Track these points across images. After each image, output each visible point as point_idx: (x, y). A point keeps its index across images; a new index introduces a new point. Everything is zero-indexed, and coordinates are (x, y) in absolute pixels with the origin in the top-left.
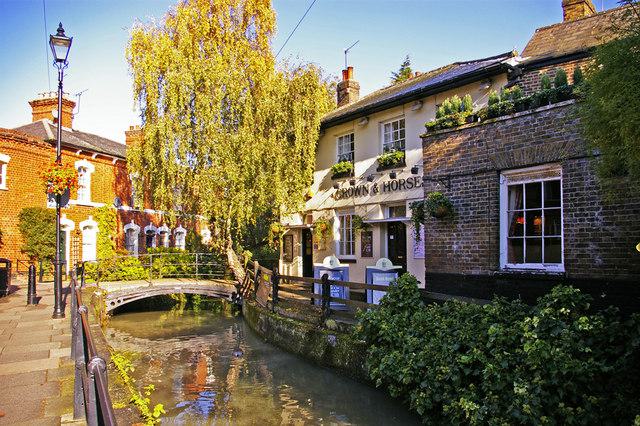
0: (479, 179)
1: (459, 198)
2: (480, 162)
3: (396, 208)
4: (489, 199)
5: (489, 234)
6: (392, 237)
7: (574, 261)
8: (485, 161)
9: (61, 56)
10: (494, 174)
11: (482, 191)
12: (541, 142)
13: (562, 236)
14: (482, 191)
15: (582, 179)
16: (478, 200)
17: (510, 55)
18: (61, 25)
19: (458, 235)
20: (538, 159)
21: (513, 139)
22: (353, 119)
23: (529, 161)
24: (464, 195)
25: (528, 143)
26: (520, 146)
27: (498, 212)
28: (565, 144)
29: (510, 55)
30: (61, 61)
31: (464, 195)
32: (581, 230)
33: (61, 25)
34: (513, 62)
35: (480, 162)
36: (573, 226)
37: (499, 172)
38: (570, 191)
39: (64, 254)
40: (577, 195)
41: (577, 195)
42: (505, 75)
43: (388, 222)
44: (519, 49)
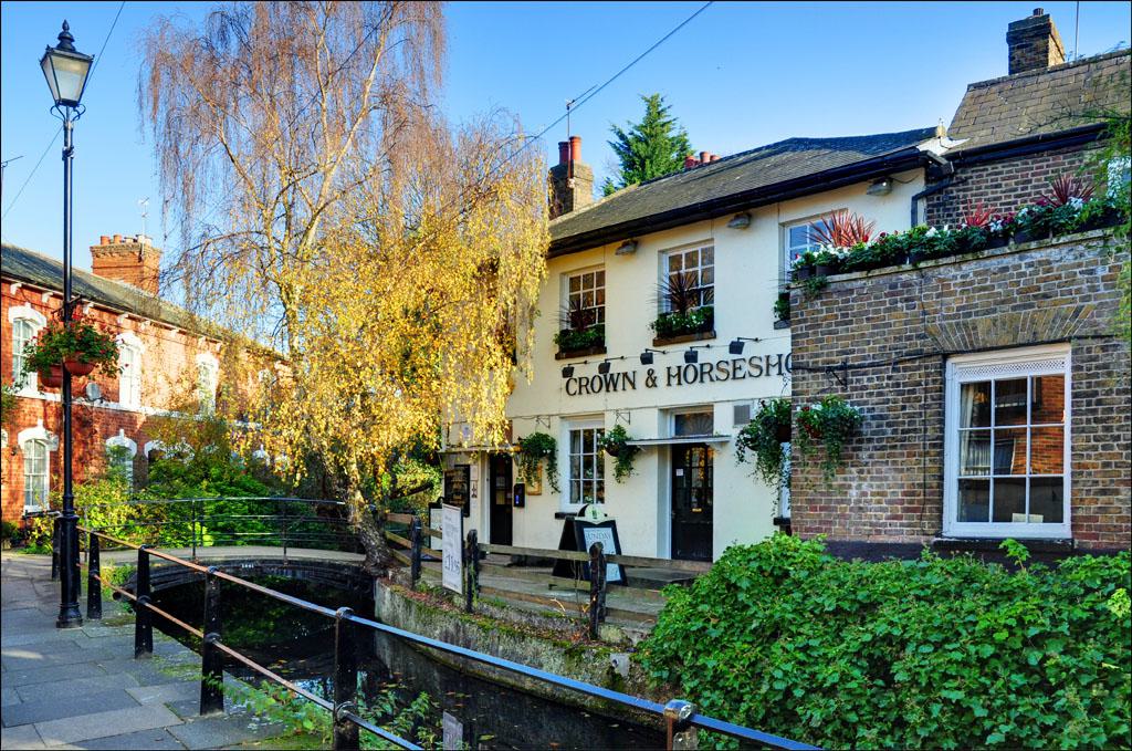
0: (905, 369)
1: (866, 403)
2: (909, 338)
3: (694, 419)
4: (925, 407)
5: (925, 470)
6: (680, 473)
7: (1088, 519)
8: (918, 337)
9: (68, 93)
10: (936, 361)
11: (913, 392)
12: (1031, 306)
13: (1067, 475)
14: (913, 392)
15: (1110, 374)
16: (904, 408)
17: (930, 133)
18: (65, 26)
19: (861, 472)
20: (1024, 336)
21: (978, 300)
22: (604, 244)
23: (1008, 340)
24: (875, 399)
25: (1007, 307)
26: (987, 312)
27: (942, 430)
28: (1077, 312)
29: (930, 133)
30: (67, 103)
31: (875, 399)
32: (1106, 465)
33: (65, 26)
34: (937, 148)
35: (909, 338)
36: (1089, 457)
37: (946, 356)
38: (1086, 395)
39: (574, 466)
40: (1099, 402)
41: (1099, 402)
42: (921, 173)
43: (674, 446)
44: (942, 118)
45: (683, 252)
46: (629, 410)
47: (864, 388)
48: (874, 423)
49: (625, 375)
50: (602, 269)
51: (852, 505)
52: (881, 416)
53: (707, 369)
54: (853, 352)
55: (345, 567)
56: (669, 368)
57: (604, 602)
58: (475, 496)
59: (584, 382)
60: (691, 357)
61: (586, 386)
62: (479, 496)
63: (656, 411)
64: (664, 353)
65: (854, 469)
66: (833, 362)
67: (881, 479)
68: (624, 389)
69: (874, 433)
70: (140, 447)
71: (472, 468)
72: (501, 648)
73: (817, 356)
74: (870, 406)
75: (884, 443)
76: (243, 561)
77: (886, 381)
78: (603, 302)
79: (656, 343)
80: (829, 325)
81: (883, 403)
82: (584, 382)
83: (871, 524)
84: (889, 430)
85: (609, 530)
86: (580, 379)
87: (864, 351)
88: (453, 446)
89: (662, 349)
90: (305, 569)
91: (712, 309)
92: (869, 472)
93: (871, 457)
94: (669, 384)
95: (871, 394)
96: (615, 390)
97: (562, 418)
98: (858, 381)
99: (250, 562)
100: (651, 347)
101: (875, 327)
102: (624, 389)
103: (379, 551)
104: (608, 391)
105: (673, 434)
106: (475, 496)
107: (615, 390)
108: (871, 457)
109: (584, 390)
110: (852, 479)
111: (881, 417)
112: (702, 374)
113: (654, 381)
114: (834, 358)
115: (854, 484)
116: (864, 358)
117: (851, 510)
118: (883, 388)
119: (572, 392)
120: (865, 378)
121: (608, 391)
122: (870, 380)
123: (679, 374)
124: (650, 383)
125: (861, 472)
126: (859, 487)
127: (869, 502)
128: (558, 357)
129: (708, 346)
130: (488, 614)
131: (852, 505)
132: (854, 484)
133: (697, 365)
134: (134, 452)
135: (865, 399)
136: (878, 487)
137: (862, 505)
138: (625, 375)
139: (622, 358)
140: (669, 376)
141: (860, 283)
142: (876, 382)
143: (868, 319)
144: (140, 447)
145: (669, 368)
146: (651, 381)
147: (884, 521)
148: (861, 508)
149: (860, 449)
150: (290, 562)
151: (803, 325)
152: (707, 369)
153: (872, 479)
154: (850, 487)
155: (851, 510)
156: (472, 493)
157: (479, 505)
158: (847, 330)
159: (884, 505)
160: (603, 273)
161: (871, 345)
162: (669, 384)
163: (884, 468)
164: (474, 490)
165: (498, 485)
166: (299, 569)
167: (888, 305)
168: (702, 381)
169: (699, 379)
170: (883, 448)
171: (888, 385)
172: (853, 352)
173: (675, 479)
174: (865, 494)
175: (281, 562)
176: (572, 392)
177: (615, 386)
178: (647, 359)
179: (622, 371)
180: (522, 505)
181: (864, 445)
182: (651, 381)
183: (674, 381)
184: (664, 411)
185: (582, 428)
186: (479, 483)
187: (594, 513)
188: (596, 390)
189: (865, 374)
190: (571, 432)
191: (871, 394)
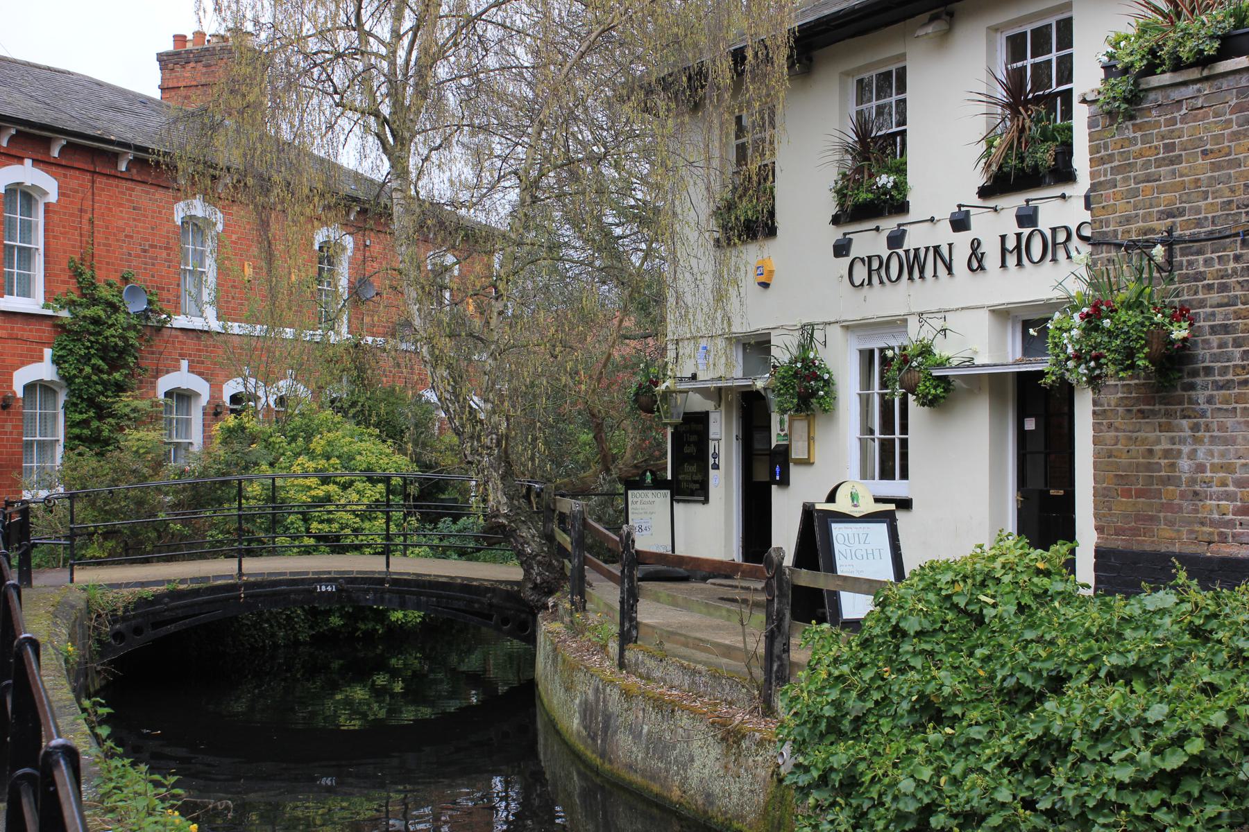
19: (1195, 428)
43: (1020, 375)
45: (1028, 29)
46: (944, 313)
47: (1199, 277)
48: (1214, 340)
49: (937, 249)
50: (900, 65)
51: (1183, 488)
52: (1226, 326)
53: (1061, 237)
54: (1181, 212)
55: (487, 590)
56: (1003, 238)
57: (787, 651)
58: (716, 467)
59: (875, 265)
60: (1027, 218)
61: (877, 270)
62: (722, 465)
63: (985, 316)
64: (995, 210)
65: (1185, 423)
66: (1152, 231)
67: (1226, 441)
68: (935, 275)
69: (1215, 358)
70: (216, 388)
71: (712, 417)
72: (646, 729)
73: (1128, 220)
74: (1208, 310)
75: (1230, 377)
76: (320, 581)
77: (1232, 265)
78: (904, 123)
79: (984, 193)
80: (1146, 165)
81: (1227, 305)
82: (875, 265)
83: (1212, 523)
84: (1237, 352)
85: (882, 529)
86: (870, 258)
87: (1198, 211)
88: (681, 379)
89: (992, 203)
90: (421, 594)
91: (1070, 129)
92: (1208, 429)
93: (1210, 400)
94: (1003, 265)
95: (1209, 288)
96: (922, 277)
97: (847, 328)
98: (1190, 263)
99: (330, 581)
100: (974, 199)
101: (1215, 167)
102: (935, 275)
103: (539, 563)
104: (911, 278)
105: (1019, 355)
106: (716, 467)
107: (922, 277)
108: (1210, 400)
109: (875, 279)
110: (1183, 441)
111: (1226, 329)
112: (1055, 244)
113: (980, 261)
114: (1155, 224)
115: (1186, 449)
116: (1199, 223)
117: (1183, 496)
118: (1228, 276)
119: (857, 283)
120: (1201, 258)
121: (911, 278)
122: (1207, 262)
123: (1018, 247)
124: (975, 265)
125: (1195, 428)
126: (1192, 455)
127: (1208, 483)
128: (836, 220)
129: (1063, 197)
130: (642, 670)
131: (1183, 488)
132: (1186, 449)
133: (901, 252)
134: (204, 399)
135: (1200, 296)
136: (1222, 455)
137: (1197, 488)
138: (937, 249)
139: (932, 220)
140: (1004, 251)
141: (1190, 90)
142: (1217, 267)
143: (1205, 153)
144: (216, 388)
145: (1003, 238)
146: (977, 261)
147: (1230, 517)
148: (1196, 493)
149: (1192, 387)
150: (395, 582)
151: (1108, 166)
152: (1061, 237)
153: (1213, 440)
154: (1180, 452)
155: (1183, 496)
156: (711, 461)
157: (723, 481)
158: (1173, 173)
159: (1231, 488)
160: (904, 68)
161: (1210, 200)
162: (1003, 265)
163: (1230, 422)
164: (716, 456)
165: (1027, 428)
166: (412, 593)
167: (1235, 128)
168: (1054, 260)
169: (1049, 256)
170: (1227, 385)
171: (1235, 271)
172: (1181, 212)
173: (1022, 435)
174: (1201, 468)
175: (381, 581)
176: (857, 283)
177: (922, 272)
178: (960, 223)
179: (932, 244)
180: (785, 482)
181: (1199, 380)
182: (977, 261)
183: (1012, 260)
184: (1002, 314)
185: (876, 344)
186: (722, 443)
187: (854, 497)
188: (1036, 259)
189: (1199, 252)
190: (861, 351)
191: (1209, 288)
